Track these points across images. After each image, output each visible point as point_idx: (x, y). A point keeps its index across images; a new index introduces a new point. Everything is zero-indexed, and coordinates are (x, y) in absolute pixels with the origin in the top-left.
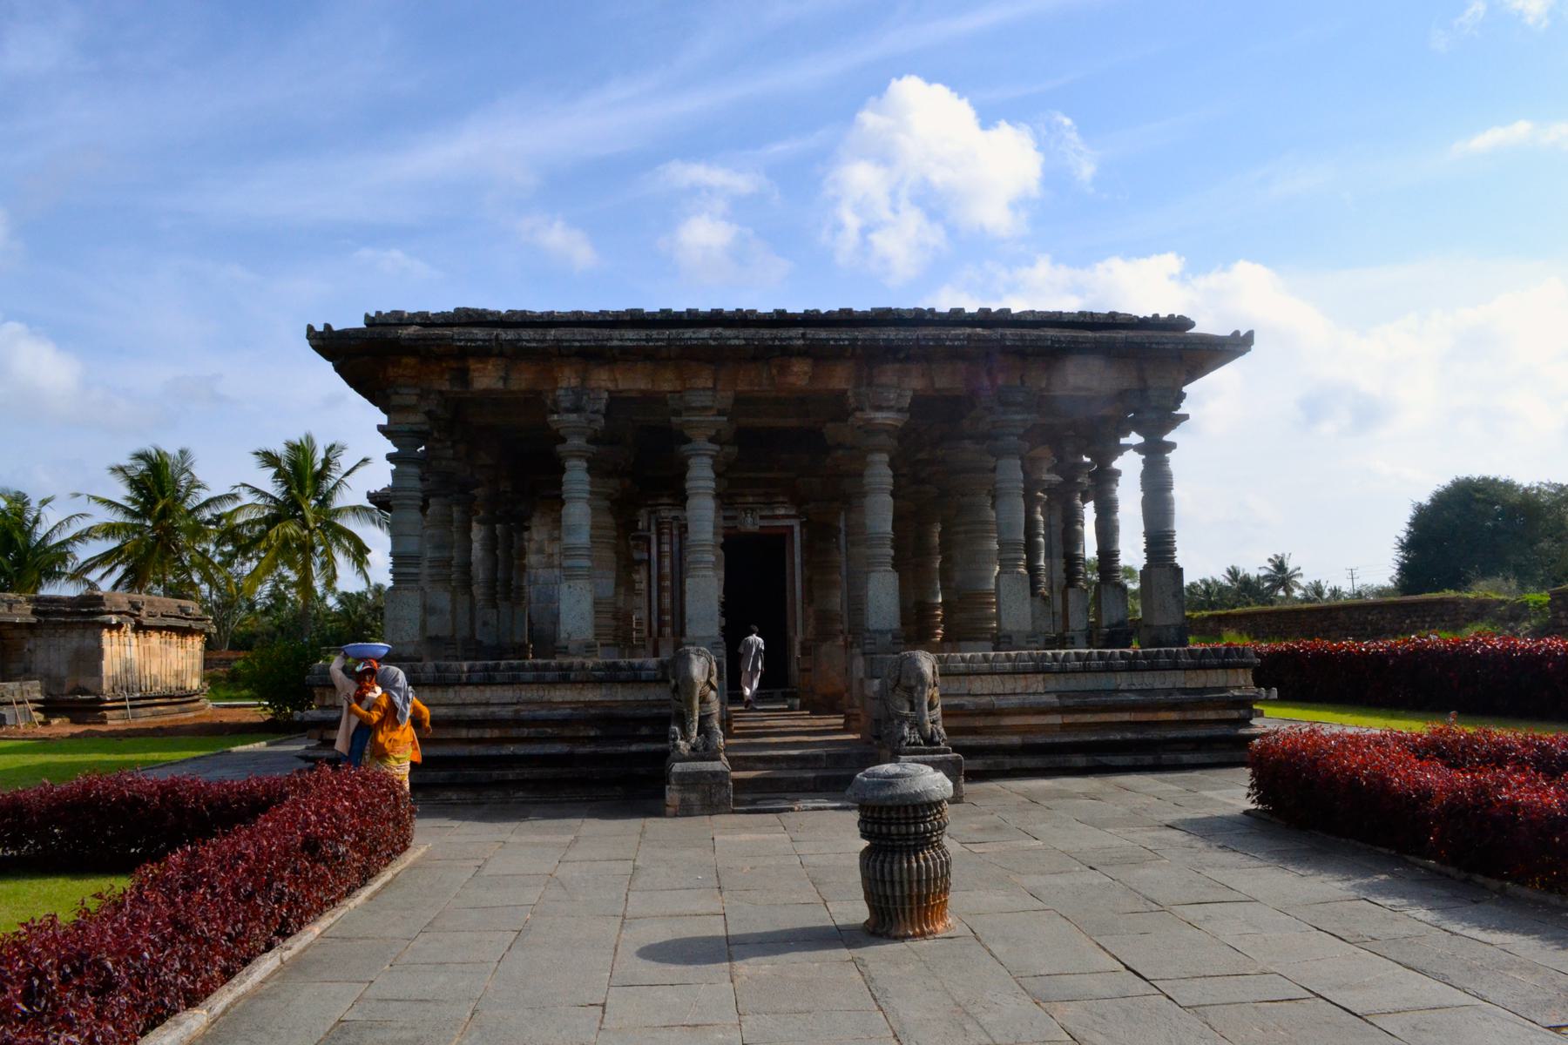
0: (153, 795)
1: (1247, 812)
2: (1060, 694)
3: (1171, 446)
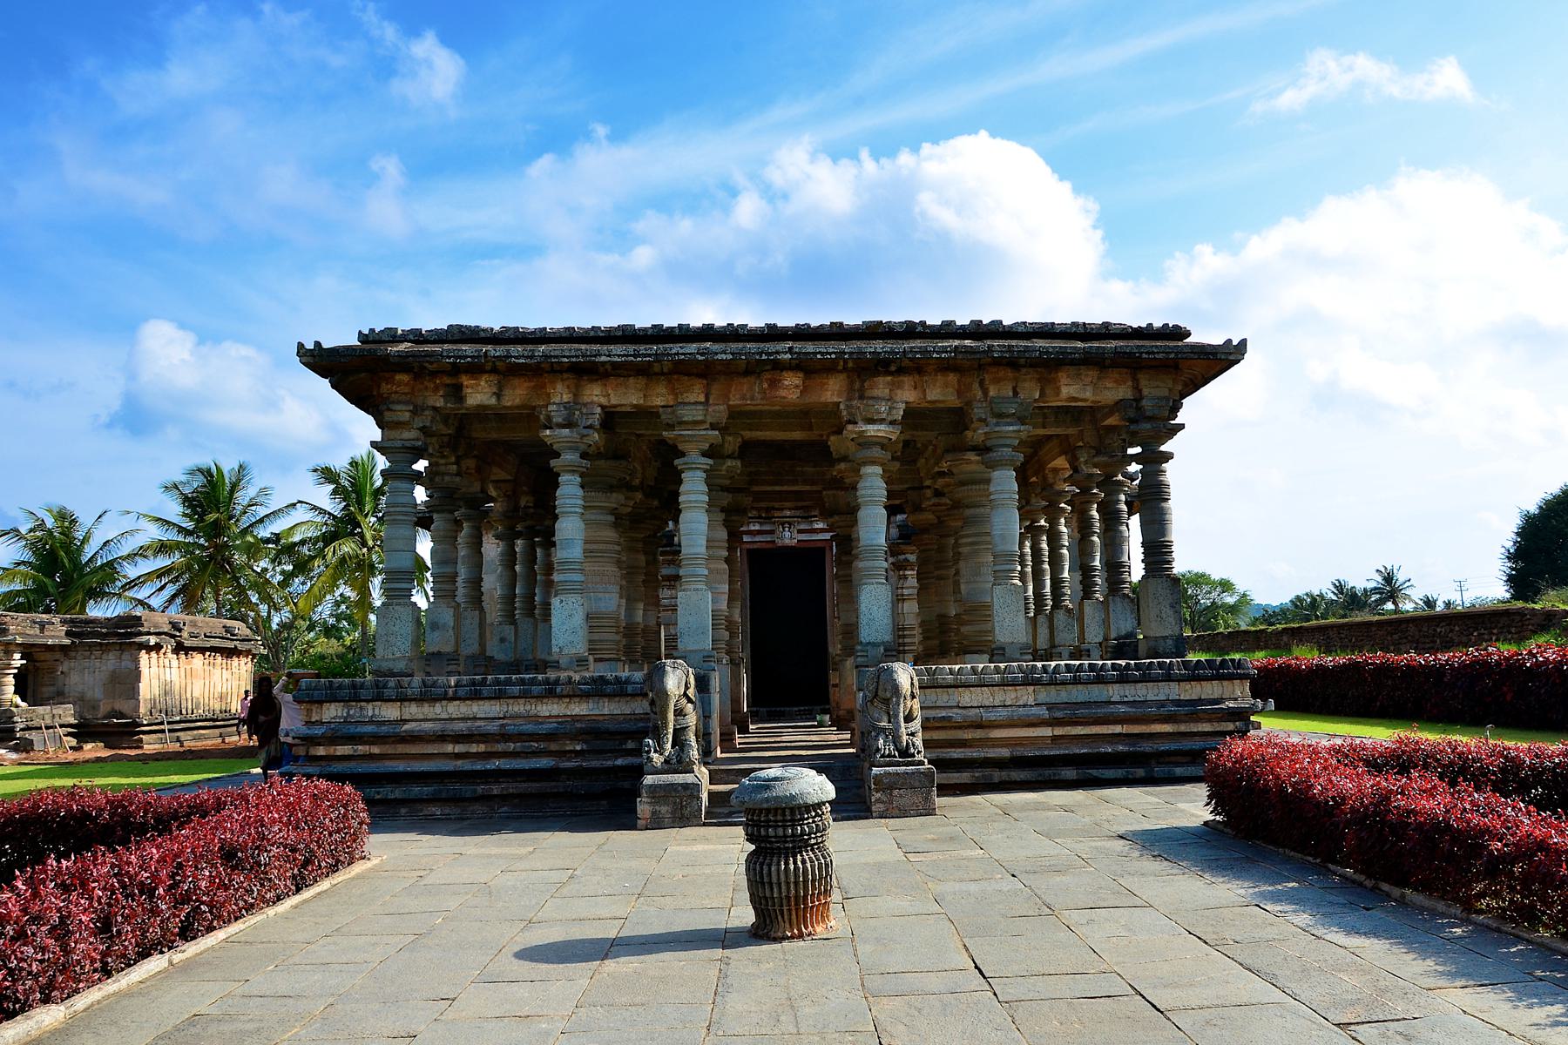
0: (101, 810)
1: (1206, 823)
2: (1051, 707)
3: (1168, 457)
